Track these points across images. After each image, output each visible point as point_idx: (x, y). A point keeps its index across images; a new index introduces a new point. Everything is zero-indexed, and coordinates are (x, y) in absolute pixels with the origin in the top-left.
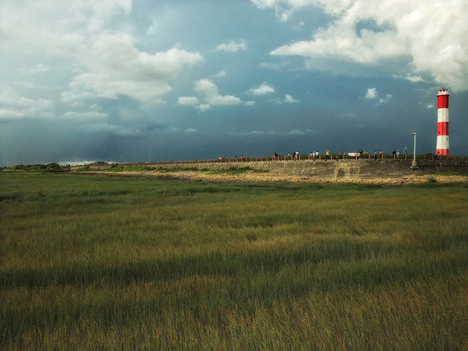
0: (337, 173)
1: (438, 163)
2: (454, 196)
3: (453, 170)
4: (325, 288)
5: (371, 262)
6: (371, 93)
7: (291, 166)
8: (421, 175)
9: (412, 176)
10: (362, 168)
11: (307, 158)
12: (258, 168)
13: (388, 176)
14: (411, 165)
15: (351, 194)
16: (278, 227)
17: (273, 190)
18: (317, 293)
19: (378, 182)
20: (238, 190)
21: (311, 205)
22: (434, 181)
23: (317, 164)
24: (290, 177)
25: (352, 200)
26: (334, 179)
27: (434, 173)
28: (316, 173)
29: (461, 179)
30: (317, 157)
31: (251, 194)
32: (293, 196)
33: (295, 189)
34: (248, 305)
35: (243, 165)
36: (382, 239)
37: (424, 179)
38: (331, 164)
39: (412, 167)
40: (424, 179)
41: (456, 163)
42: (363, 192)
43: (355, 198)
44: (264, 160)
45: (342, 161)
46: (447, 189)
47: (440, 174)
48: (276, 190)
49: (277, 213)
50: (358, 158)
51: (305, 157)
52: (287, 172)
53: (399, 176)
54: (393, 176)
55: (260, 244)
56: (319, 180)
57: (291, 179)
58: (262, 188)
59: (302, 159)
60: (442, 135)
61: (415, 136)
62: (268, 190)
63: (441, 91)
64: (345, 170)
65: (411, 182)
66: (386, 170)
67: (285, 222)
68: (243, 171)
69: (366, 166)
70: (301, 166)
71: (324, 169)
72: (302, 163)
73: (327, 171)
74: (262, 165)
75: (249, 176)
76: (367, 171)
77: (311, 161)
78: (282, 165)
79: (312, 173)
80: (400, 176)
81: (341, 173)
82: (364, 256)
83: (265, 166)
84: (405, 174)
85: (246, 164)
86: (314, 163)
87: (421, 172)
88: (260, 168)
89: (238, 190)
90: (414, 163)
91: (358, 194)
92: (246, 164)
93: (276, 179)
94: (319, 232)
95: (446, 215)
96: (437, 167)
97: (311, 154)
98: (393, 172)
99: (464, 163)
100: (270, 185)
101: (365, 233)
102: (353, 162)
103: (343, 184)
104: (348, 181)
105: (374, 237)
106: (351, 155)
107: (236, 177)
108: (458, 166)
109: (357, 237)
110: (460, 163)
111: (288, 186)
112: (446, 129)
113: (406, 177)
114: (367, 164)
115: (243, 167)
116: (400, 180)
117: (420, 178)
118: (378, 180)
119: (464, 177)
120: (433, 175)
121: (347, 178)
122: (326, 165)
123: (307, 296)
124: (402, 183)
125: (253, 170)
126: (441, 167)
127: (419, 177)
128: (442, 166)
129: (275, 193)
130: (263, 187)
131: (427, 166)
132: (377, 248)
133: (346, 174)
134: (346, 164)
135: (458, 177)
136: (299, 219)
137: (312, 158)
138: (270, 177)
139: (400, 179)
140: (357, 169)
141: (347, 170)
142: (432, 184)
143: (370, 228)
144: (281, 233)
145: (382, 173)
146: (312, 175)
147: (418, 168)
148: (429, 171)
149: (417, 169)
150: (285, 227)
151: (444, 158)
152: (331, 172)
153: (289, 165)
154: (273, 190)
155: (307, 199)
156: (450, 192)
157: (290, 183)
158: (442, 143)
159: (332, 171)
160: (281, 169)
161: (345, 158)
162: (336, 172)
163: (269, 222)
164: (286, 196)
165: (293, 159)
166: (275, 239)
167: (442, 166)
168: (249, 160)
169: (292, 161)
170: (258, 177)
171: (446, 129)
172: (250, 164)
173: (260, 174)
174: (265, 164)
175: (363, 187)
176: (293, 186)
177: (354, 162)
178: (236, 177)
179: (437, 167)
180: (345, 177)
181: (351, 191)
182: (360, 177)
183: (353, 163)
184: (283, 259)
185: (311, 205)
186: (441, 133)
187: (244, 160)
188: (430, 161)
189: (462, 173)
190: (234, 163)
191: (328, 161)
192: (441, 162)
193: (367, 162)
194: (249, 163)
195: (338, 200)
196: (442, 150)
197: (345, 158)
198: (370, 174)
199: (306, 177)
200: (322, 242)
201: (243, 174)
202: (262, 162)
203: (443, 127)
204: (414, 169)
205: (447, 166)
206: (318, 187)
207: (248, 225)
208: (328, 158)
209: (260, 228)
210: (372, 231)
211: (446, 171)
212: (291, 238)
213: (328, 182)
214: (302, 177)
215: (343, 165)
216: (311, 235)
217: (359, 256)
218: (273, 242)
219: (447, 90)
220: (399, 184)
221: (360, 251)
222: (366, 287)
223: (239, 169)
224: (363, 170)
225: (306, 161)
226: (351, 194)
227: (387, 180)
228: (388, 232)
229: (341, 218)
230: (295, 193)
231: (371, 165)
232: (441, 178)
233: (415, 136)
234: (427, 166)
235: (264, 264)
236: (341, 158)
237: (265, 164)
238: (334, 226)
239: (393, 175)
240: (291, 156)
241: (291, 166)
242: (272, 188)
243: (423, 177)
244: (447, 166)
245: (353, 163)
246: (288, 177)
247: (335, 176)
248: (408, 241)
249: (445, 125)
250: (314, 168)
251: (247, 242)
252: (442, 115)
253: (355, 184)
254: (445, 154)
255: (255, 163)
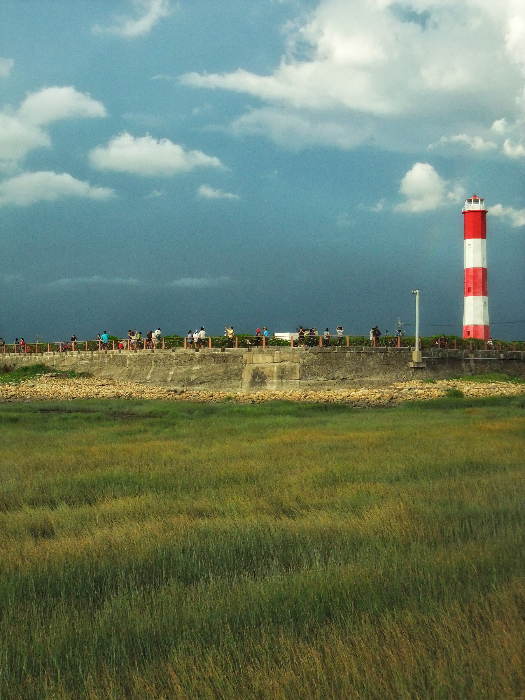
0: (250, 378)
1: (466, 356)
2: (497, 425)
3: (497, 371)
4: (209, 637)
5: (314, 573)
6: (420, 177)
7: (143, 362)
8: (431, 381)
9: (414, 383)
10: (304, 366)
11: (181, 345)
12: (65, 366)
13: (362, 384)
14: (409, 358)
15: (279, 426)
16: (107, 506)
17: (98, 419)
18: (188, 651)
19: (339, 397)
20: (15, 420)
21: (186, 451)
22: (458, 394)
23: (203, 357)
24: (142, 387)
25: (276, 439)
26: (242, 391)
27: (458, 378)
28: (202, 379)
29: (513, 389)
30: (203, 342)
31: (46, 429)
32: (145, 431)
33: (150, 415)
34: (25, 689)
35: (28, 360)
36: (339, 524)
37: (437, 389)
38: (236, 357)
39: (411, 365)
40: (437, 389)
41: (502, 356)
42: (306, 420)
43: (287, 434)
44: (79, 348)
45: (260, 351)
46: (484, 410)
47: (470, 379)
48: (108, 419)
49: (101, 472)
50: (295, 343)
51: (175, 342)
52: (134, 376)
53: (384, 384)
54: (371, 385)
55: (63, 545)
56: (209, 394)
57: (143, 392)
58: (73, 414)
59: (168, 346)
60: (475, 294)
61: (417, 297)
62: (88, 419)
63: (470, 201)
64: (267, 372)
65: (410, 397)
66: (356, 370)
67: (123, 495)
68: (30, 375)
69: (313, 363)
70: (166, 362)
71: (220, 369)
72: (168, 357)
73: (225, 373)
74: (74, 360)
75: (44, 387)
76: (316, 374)
77: (191, 351)
78: (122, 361)
79: (193, 378)
80: (386, 383)
81: (259, 378)
82: (299, 562)
83: (82, 362)
84: (397, 380)
85: (36, 358)
86: (197, 355)
87: (431, 375)
88: (71, 368)
89: (15, 420)
90: (416, 355)
91: (295, 426)
92: (36, 358)
93: (107, 392)
94: (201, 514)
95: (474, 467)
96: (463, 364)
97: (189, 336)
98: (371, 375)
99: (519, 355)
100: (92, 407)
101: (304, 512)
102: (285, 352)
103: (263, 403)
104: (273, 395)
105: (323, 520)
106: (280, 338)
107: (12, 389)
108: (507, 362)
109: (286, 522)
110: (511, 355)
111: (137, 409)
112: (481, 282)
113: (399, 385)
114: (315, 357)
115: (29, 364)
116: (387, 393)
117: (429, 389)
118: (340, 393)
119: (519, 385)
120: (455, 381)
121: (273, 390)
122: (224, 360)
123: (166, 660)
124: (392, 398)
125: (52, 371)
126: (473, 364)
127: (427, 385)
128: (475, 361)
129: (103, 426)
130: (77, 411)
131: (442, 362)
132: (328, 541)
133: (269, 381)
134: (269, 359)
135: (506, 384)
136: (160, 486)
137: (192, 344)
138: (94, 390)
139: (387, 390)
140: (293, 369)
141: (271, 371)
142: (455, 401)
143: (316, 500)
144: (113, 519)
145: (349, 377)
146: (191, 384)
147: (424, 365)
148: (448, 371)
149: (423, 368)
150: (121, 504)
151: (478, 344)
152: (237, 375)
153: (138, 360)
154: (98, 419)
155: (177, 437)
156: (490, 418)
157: (141, 402)
158: (474, 312)
159: (238, 374)
160: (120, 370)
161: (266, 344)
162: (247, 377)
163: (86, 494)
164: (129, 433)
165: (148, 347)
166: (98, 532)
167: (475, 361)
168: (43, 349)
169: (145, 352)
170: (66, 389)
171: (481, 282)
172: (46, 357)
173: (71, 381)
174: (81, 359)
175: (306, 409)
176: (145, 409)
177: (287, 352)
178: (12, 389)
179: (463, 364)
180: (268, 387)
181: (280, 419)
182: (301, 385)
183: (286, 356)
184: (115, 577)
185: (186, 451)
186: (472, 290)
187: (32, 349)
188: (450, 352)
189: (513, 378)
190: (7, 357)
191: (229, 351)
192: (472, 352)
193: (315, 354)
194: (45, 356)
195: (248, 441)
196: (476, 327)
197: (266, 344)
198: (321, 379)
199: (179, 388)
200: (205, 535)
201: (30, 383)
202: (75, 354)
203: (475, 277)
204: (417, 368)
205: (483, 362)
206: (207, 410)
207: (33, 503)
208: (230, 343)
209: (64, 508)
210: (320, 507)
211: (482, 372)
212: (136, 530)
213: (229, 398)
214: (168, 388)
215: (262, 359)
216: (182, 521)
217: (289, 564)
218: (93, 539)
219: (482, 200)
220: (385, 400)
221: (288, 553)
222: (299, 631)
223: (18, 371)
224: (306, 371)
225: (179, 350)
226: (279, 426)
227: (360, 392)
228: (355, 509)
229: (253, 479)
230: (152, 425)
231: (325, 360)
232: (471, 388)
233: (417, 297)
234: (442, 362)
235: (68, 593)
236: (258, 343)
237: (81, 359)
238: (234, 499)
239: (373, 383)
240: (144, 341)
241: (143, 362)
242: (95, 415)
243: (435, 385)
244: (483, 362)
245: (286, 356)
246: (137, 388)
247: (246, 385)
248: (396, 525)
249: (480, 274)
250: (196, 368)
251: (29, 544)
252: (474, 254)
253: (288, 403)
254: (481, 336)
255: (57, 355)
